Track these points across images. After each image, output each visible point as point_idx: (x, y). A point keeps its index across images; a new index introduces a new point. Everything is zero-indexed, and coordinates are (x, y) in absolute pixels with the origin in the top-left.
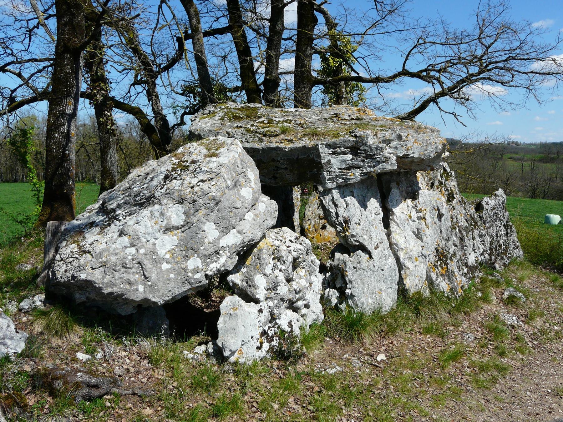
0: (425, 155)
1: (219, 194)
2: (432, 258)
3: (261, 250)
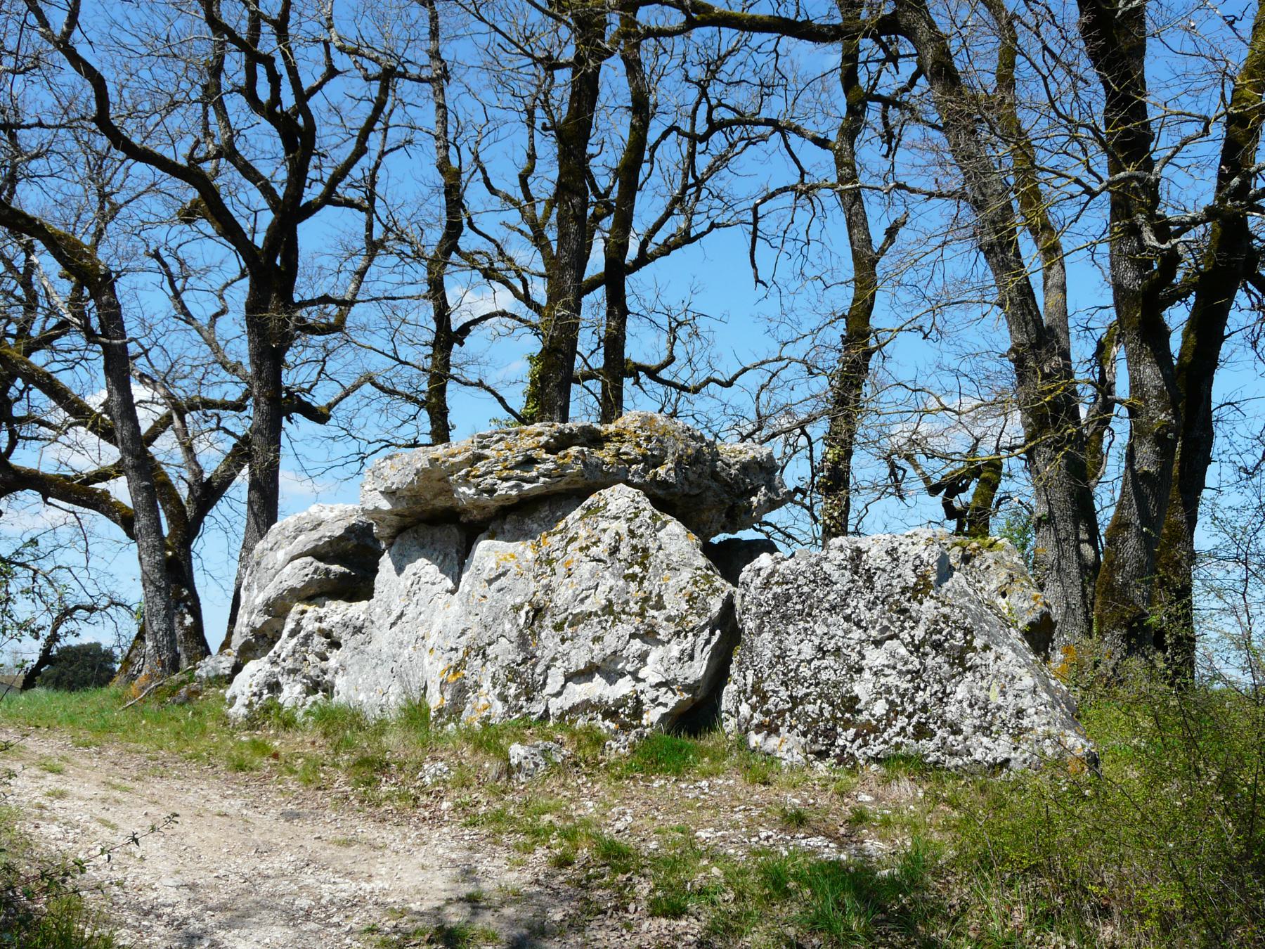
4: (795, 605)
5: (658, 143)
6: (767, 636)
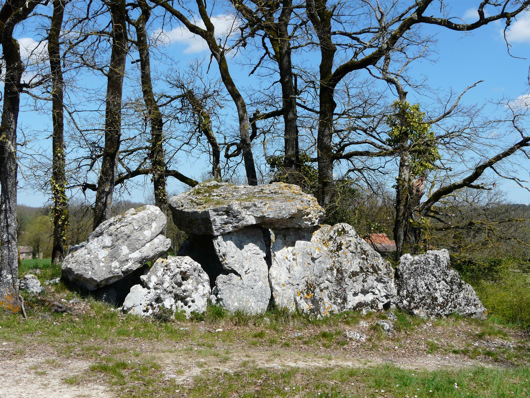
0: (278, 216)
1: (129, 232)
2: (302, 287)
3: (157, 263)
4: (419, 271)
5: (31, 94)
6: (412, 280)
